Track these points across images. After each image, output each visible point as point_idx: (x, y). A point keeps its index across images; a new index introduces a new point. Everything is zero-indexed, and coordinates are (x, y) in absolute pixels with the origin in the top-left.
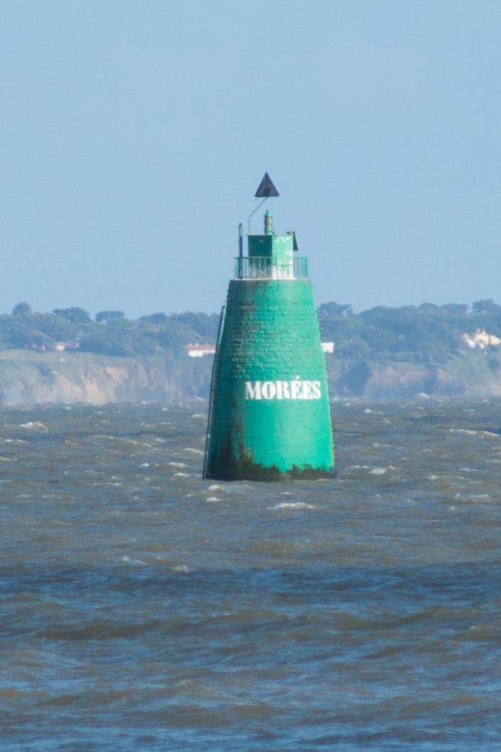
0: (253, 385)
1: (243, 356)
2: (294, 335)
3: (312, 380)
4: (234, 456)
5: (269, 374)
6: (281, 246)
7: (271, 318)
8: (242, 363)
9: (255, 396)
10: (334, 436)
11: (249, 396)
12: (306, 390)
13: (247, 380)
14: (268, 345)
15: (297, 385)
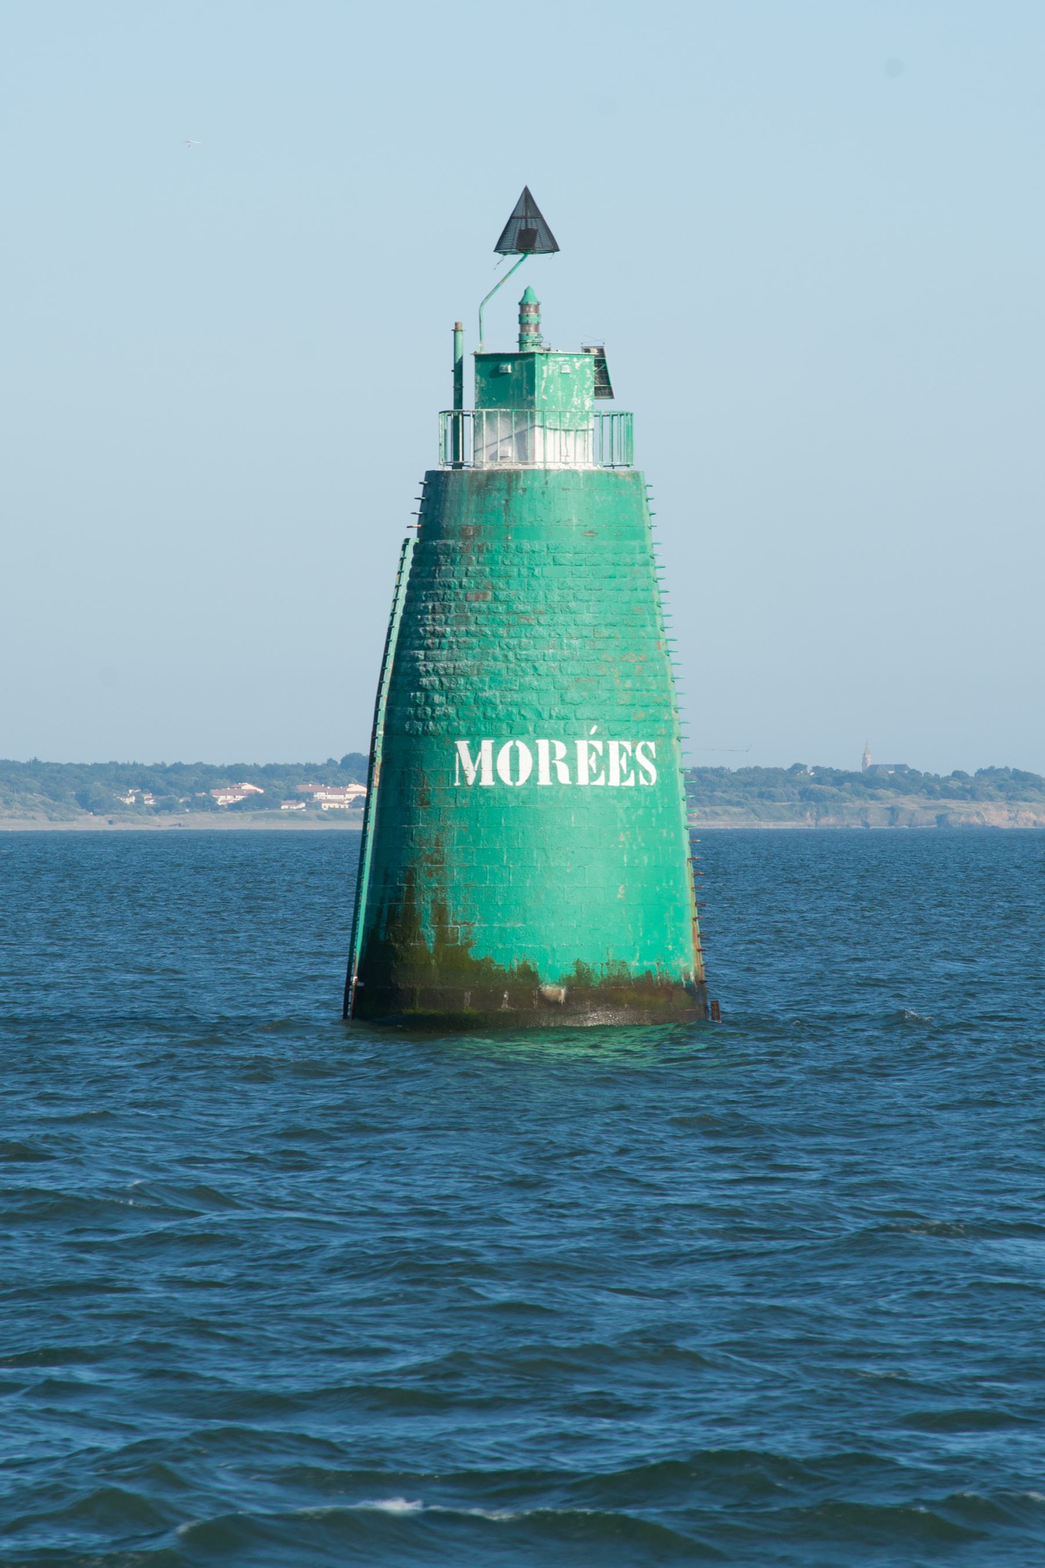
0: (475, 750)
1: (451, 671)
2: (587, 618)
3: (635, 739)
4: (421, 937)
5: (517, 718)
6: (562, 377)
7: (524, 571)
8: (446, 691)
9: (478, 778)
10: (696, 888)
11: (463, 777)
12: (616, 763)
13: (459, 736)
14: (514, 642)
15: (592, 749)
